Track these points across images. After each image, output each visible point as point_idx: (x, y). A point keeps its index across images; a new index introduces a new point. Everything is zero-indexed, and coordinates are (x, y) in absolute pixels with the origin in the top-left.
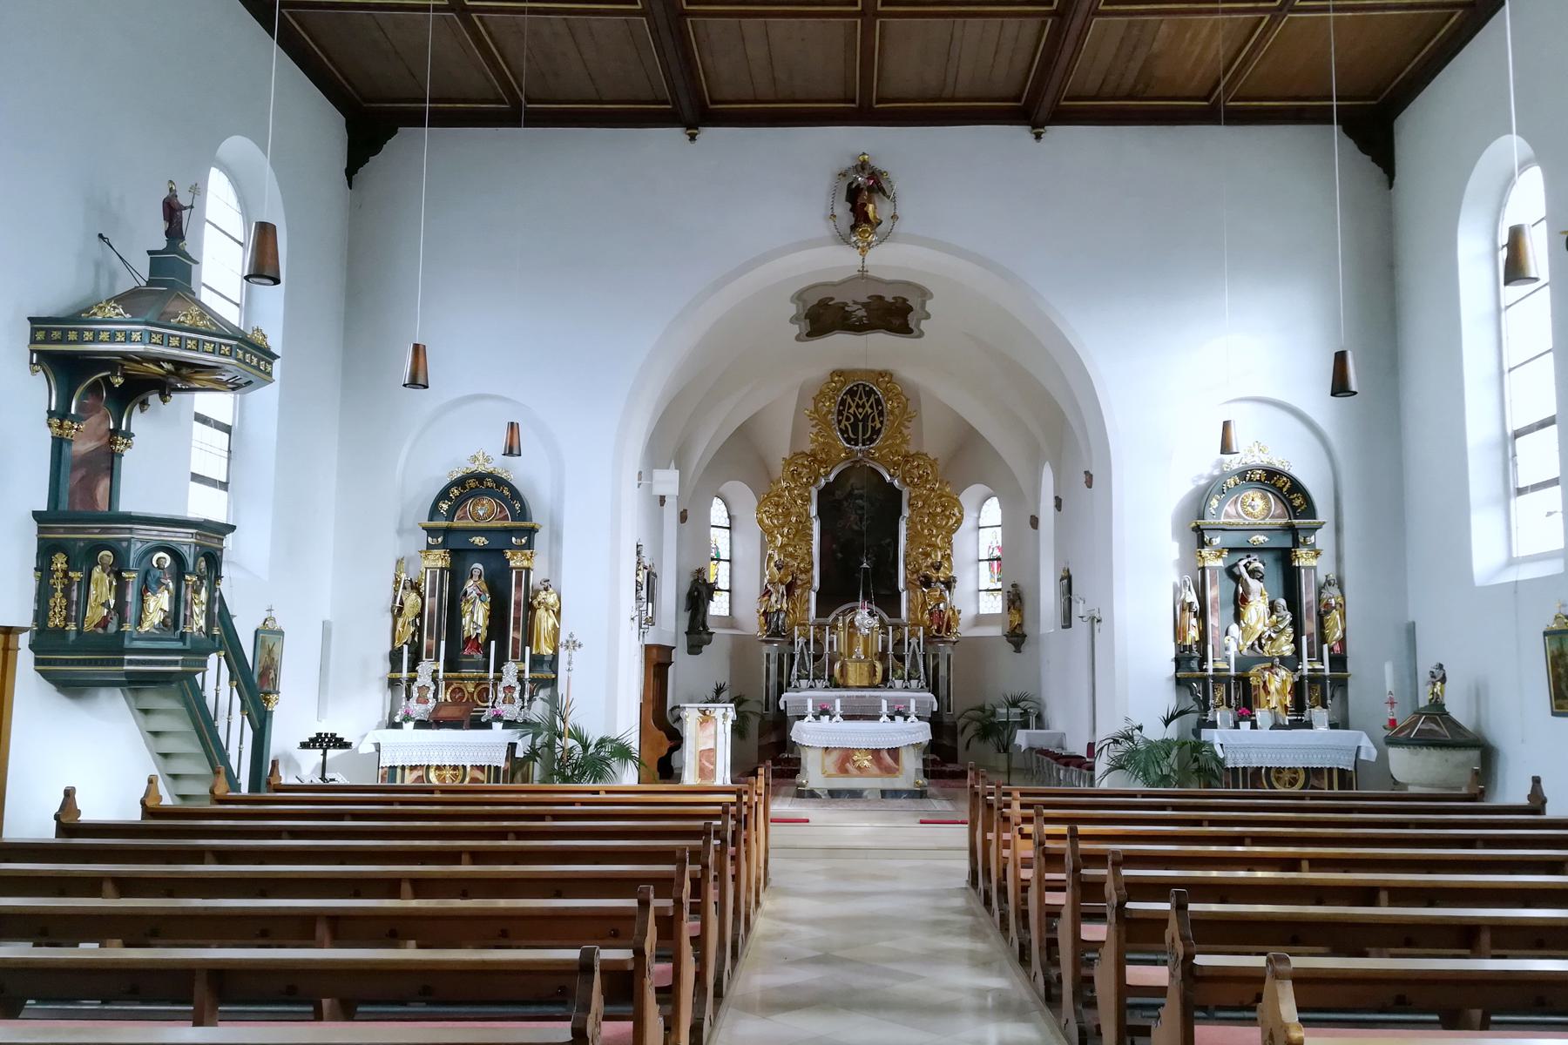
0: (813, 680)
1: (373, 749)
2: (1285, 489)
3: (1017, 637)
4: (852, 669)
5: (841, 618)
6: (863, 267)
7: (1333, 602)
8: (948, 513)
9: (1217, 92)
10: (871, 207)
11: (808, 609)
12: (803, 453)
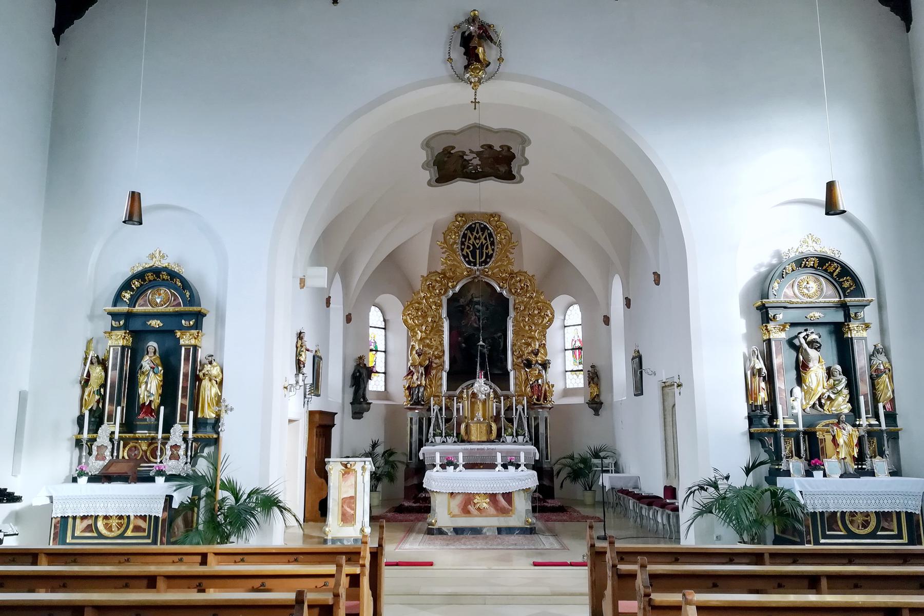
0: (445, 437)
1: (48, 501)
2: (835, 274)
3: (596, 404)
4: (474, 428)
5: (465, 391)
6: (475, 99)
7: (882, 367)
8: (543, 314)
10: (481, 49)
11: (441, 385)
12: (436, 272)
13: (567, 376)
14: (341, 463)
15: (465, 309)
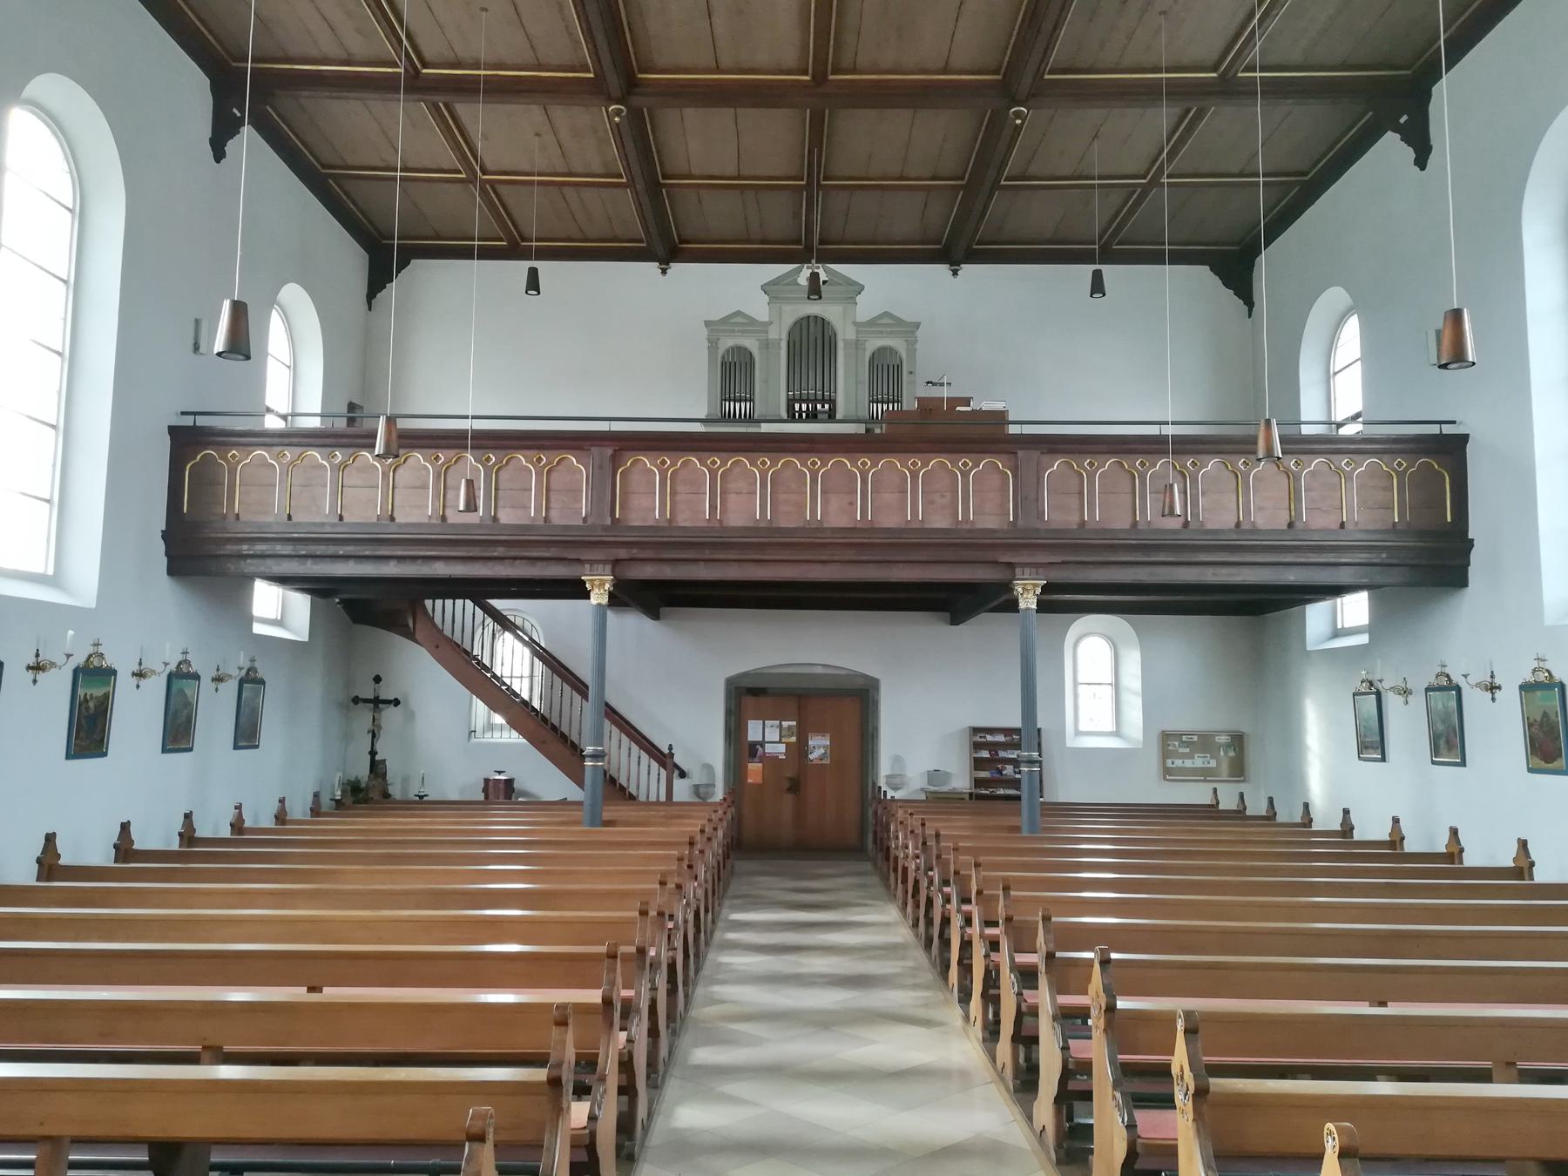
9: (1162, 157)
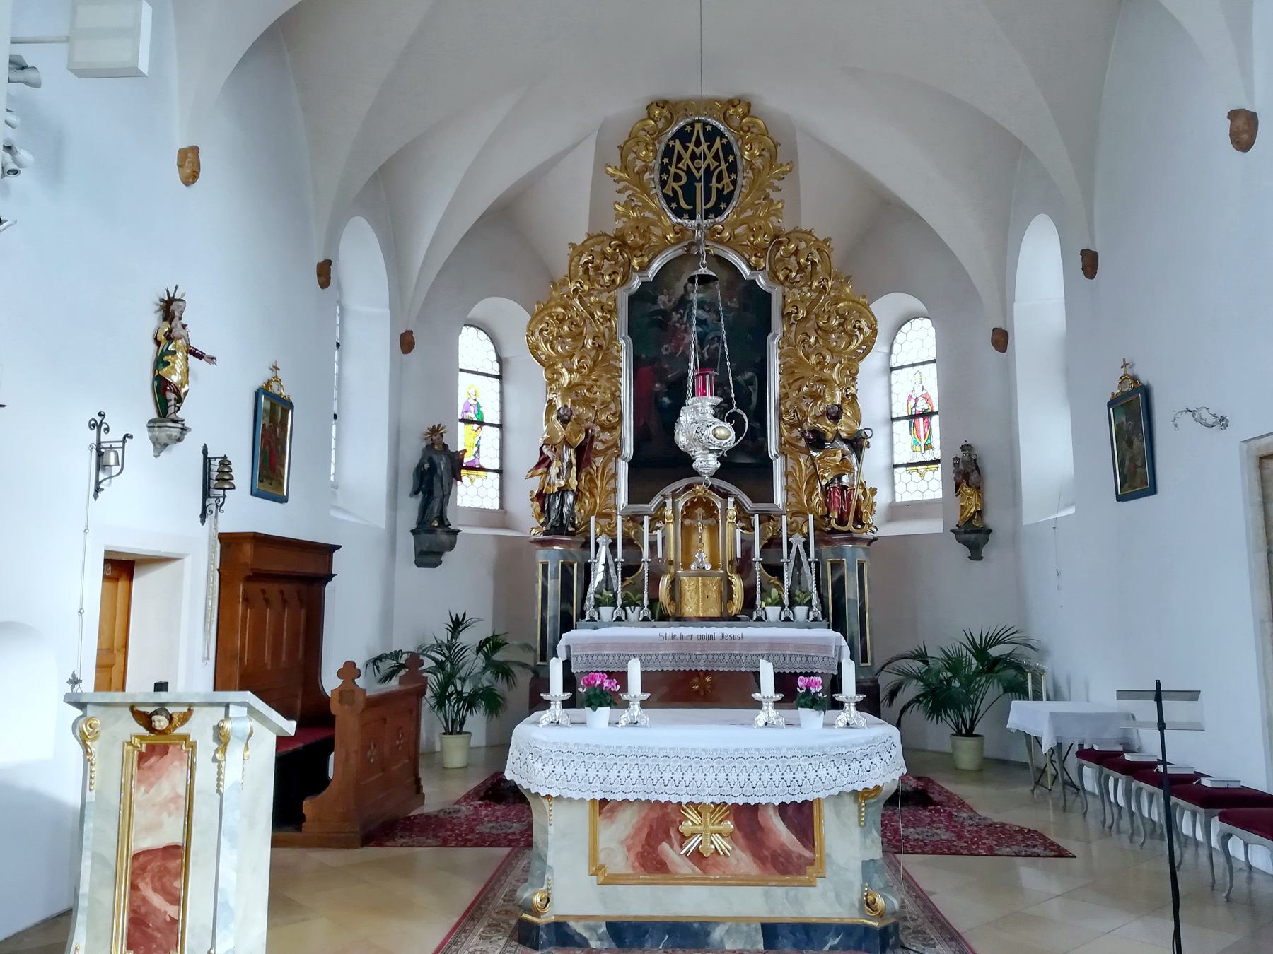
0: (623, 607)
5: (669, 501)
8: (850, 327)
11: (615, 491)
13: (896, 475)
14: (132, 708)
15: (670, 319)
